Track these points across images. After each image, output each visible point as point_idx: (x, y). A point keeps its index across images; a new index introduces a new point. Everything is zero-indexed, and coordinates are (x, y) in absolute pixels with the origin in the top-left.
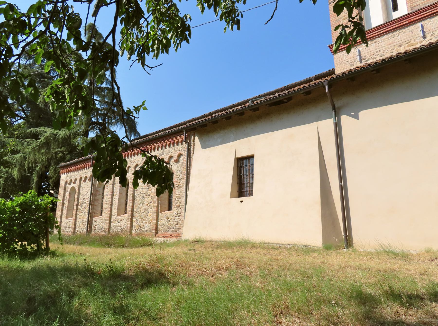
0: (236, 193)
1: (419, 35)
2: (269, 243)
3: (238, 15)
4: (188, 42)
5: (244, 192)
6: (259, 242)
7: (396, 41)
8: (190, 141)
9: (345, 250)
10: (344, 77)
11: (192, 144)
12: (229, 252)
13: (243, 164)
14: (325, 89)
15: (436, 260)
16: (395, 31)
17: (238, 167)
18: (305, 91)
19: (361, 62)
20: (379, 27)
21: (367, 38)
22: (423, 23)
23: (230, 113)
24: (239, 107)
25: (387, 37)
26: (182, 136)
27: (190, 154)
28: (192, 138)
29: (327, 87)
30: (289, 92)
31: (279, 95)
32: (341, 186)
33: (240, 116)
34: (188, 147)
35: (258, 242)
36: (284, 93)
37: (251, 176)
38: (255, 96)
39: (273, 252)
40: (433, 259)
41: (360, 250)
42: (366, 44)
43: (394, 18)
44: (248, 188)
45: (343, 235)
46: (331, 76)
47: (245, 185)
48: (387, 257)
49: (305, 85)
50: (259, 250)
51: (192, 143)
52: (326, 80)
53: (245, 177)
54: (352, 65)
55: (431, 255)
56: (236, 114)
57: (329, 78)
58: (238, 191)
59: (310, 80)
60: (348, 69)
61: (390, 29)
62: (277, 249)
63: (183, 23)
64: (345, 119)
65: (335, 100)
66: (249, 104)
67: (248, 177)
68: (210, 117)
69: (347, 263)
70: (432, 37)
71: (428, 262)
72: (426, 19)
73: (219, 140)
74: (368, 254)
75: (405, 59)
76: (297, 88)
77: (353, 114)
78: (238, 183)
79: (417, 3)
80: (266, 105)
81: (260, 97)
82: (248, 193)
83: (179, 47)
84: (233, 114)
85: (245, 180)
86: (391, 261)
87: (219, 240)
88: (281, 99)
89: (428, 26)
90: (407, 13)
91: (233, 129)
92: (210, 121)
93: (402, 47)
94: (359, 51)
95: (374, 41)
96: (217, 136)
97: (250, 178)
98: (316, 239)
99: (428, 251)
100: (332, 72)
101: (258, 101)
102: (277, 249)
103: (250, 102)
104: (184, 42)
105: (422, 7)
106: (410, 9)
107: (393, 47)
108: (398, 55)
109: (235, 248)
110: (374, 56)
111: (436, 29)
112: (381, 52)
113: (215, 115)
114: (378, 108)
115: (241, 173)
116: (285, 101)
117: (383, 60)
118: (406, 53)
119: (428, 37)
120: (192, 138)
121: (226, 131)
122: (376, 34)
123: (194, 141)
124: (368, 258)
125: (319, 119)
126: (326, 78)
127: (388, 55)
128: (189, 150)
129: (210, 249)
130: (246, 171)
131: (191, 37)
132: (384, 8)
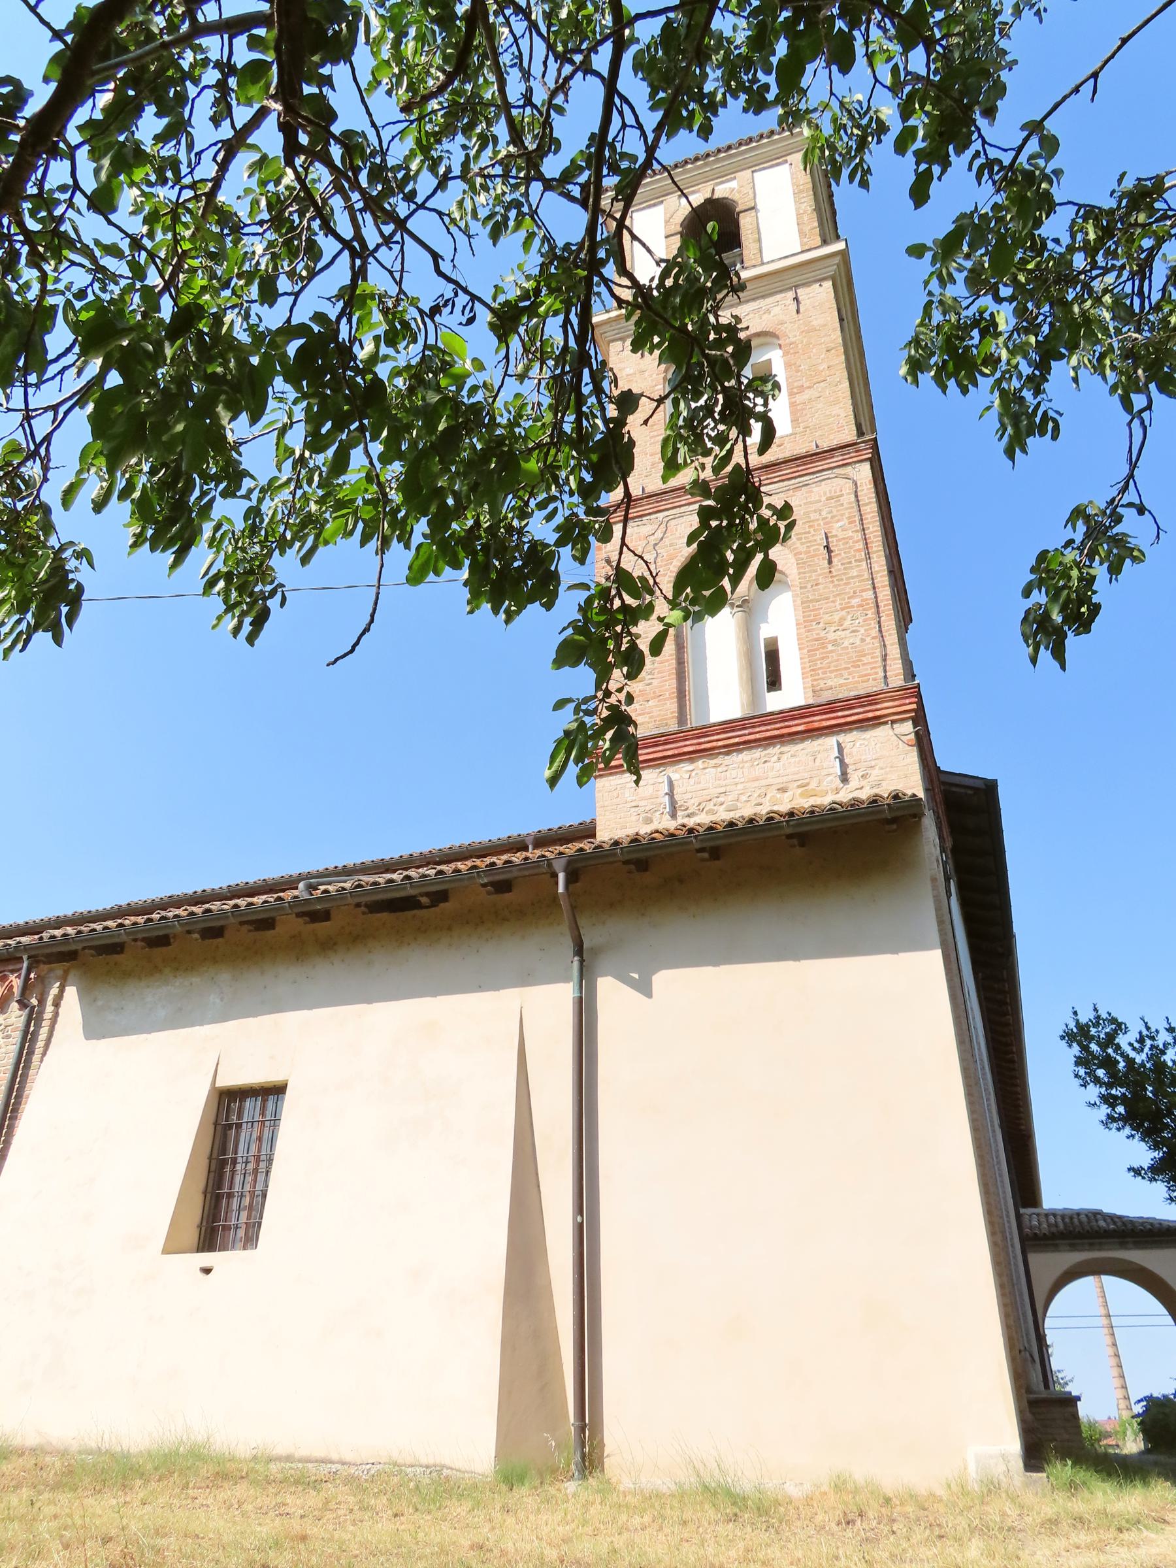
0: (191, 1234)
1: (831, 771)
2: (289, 1458)
3: (273, 593)
4: (58, 639)
5: (226, 1228)
6: (248, 1456)
7: (771, 774)
8: (42, 1002)
9: (571, 1487)
10: (615, 854)
11: (48, 1015)
12: (100, 1508)
13: (240, 1117)
14: (557, 883)
15: (858, 1522)
16: (769, 745)
17: (216, 1124)
18: (491, 879)
19: (673, 815)
20: (729, 726)
21: (641, 758)
22: (841, 738)
23: (222, 914)
24: (258, 900)
25: (749, 757)
26: (12, 977)
27: (31, 1053)
28: (54, 991)
29: (561, 877)
30: (441, 872)
31: (408, 878)
32: (579, 1228)
33: (257, 929)
34: (28, 1025)
35: (244, 1451)
36: (424, 876)
37: (263, 1165)
38: (331, 866)
39: (295, 1501)
40: (850, 1517)
41: (627, 1484)
42: (635, 778)
43: (769, 709)
44: (244, 1215)
45: (572, 1420)
46: (578, 845)
47: (235, 1201)
48: (711, 1512)
49: (494, 859)
50: (241, 1490)
51: (49, 1008)
52: (561, 853)
53: (238, 1167)
54: (648, 821)
55: (846, 1504)
56: (242, 923)
57: (570, 849)
58: (200, 1227)
59: (519, 845)
60: (631, 831)
61: (758, 736)
62: (316, 1484)
63: (59, 572)
64: (608, 988)
65: (582, 922)
66: (296, 892)
67: (250, 1166)
68: (140, 919)
69: (565, 1548)
70: (863, 783)
71: (836, 1529)
72: (851, 730)
73: (162, 1013)
74: (652, 1498)
75: (789, 831)
76: (469, 863)
77: (636, 976)
78: (205, 1193)
79: (830, 683)
80: (358, 905)
81: (347, 872)
82: (241, 1233)
83: (20, 646)
84: (232, 920)
85: (238, 1179)
86: (720, 1529)
87: (74, 1447)
88: (412, 892)
89: (854, 749)
90: (802, 703)
91: (225, 976)
92: (140, 936)
93: (786, 795)
94: (671, 783)
95: (713, 762)
96: (155, 995)
97: (256, 1171)
98: (469, 1439)
99: (839, 1486)
100: (588, 831)
101: (330, 888)
102: (316, 1484)
103: (301, 885)
104: (43, 638)
105: (840, 696)
106: (811, 694)
107: (763, 790)
108: (772, 818)
109: (139, 1482)
110: (710, 806)
111: (873, 763)
112: (730, 798)
113: (163, 913)
114: (710, 968)
115: (224, 1151)
116: (424, 900)
117: (731, 824)
118: (791, 814)
119: (854, 782)
120: (54, 991)
121: (196, 980)
122: (720, 743)
123: (57, 1005)
124: (647, 1519)
125: (526, 978)
126: (561, 849)
127: (747, 812)
128: (28, 1038)
129: (25, 1493)
130: (245, 1144)
131: (76, 626)
132: (745, 676)
